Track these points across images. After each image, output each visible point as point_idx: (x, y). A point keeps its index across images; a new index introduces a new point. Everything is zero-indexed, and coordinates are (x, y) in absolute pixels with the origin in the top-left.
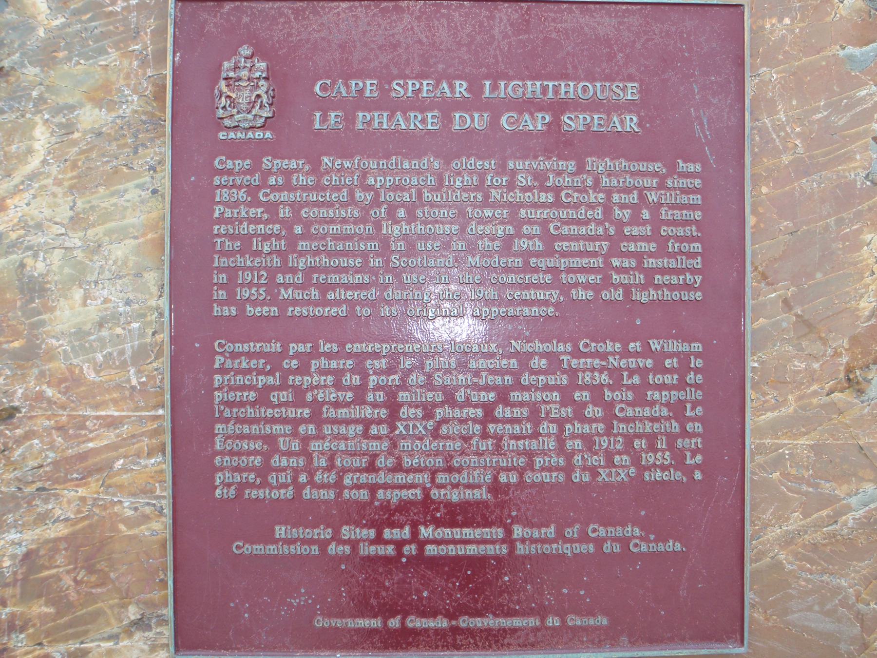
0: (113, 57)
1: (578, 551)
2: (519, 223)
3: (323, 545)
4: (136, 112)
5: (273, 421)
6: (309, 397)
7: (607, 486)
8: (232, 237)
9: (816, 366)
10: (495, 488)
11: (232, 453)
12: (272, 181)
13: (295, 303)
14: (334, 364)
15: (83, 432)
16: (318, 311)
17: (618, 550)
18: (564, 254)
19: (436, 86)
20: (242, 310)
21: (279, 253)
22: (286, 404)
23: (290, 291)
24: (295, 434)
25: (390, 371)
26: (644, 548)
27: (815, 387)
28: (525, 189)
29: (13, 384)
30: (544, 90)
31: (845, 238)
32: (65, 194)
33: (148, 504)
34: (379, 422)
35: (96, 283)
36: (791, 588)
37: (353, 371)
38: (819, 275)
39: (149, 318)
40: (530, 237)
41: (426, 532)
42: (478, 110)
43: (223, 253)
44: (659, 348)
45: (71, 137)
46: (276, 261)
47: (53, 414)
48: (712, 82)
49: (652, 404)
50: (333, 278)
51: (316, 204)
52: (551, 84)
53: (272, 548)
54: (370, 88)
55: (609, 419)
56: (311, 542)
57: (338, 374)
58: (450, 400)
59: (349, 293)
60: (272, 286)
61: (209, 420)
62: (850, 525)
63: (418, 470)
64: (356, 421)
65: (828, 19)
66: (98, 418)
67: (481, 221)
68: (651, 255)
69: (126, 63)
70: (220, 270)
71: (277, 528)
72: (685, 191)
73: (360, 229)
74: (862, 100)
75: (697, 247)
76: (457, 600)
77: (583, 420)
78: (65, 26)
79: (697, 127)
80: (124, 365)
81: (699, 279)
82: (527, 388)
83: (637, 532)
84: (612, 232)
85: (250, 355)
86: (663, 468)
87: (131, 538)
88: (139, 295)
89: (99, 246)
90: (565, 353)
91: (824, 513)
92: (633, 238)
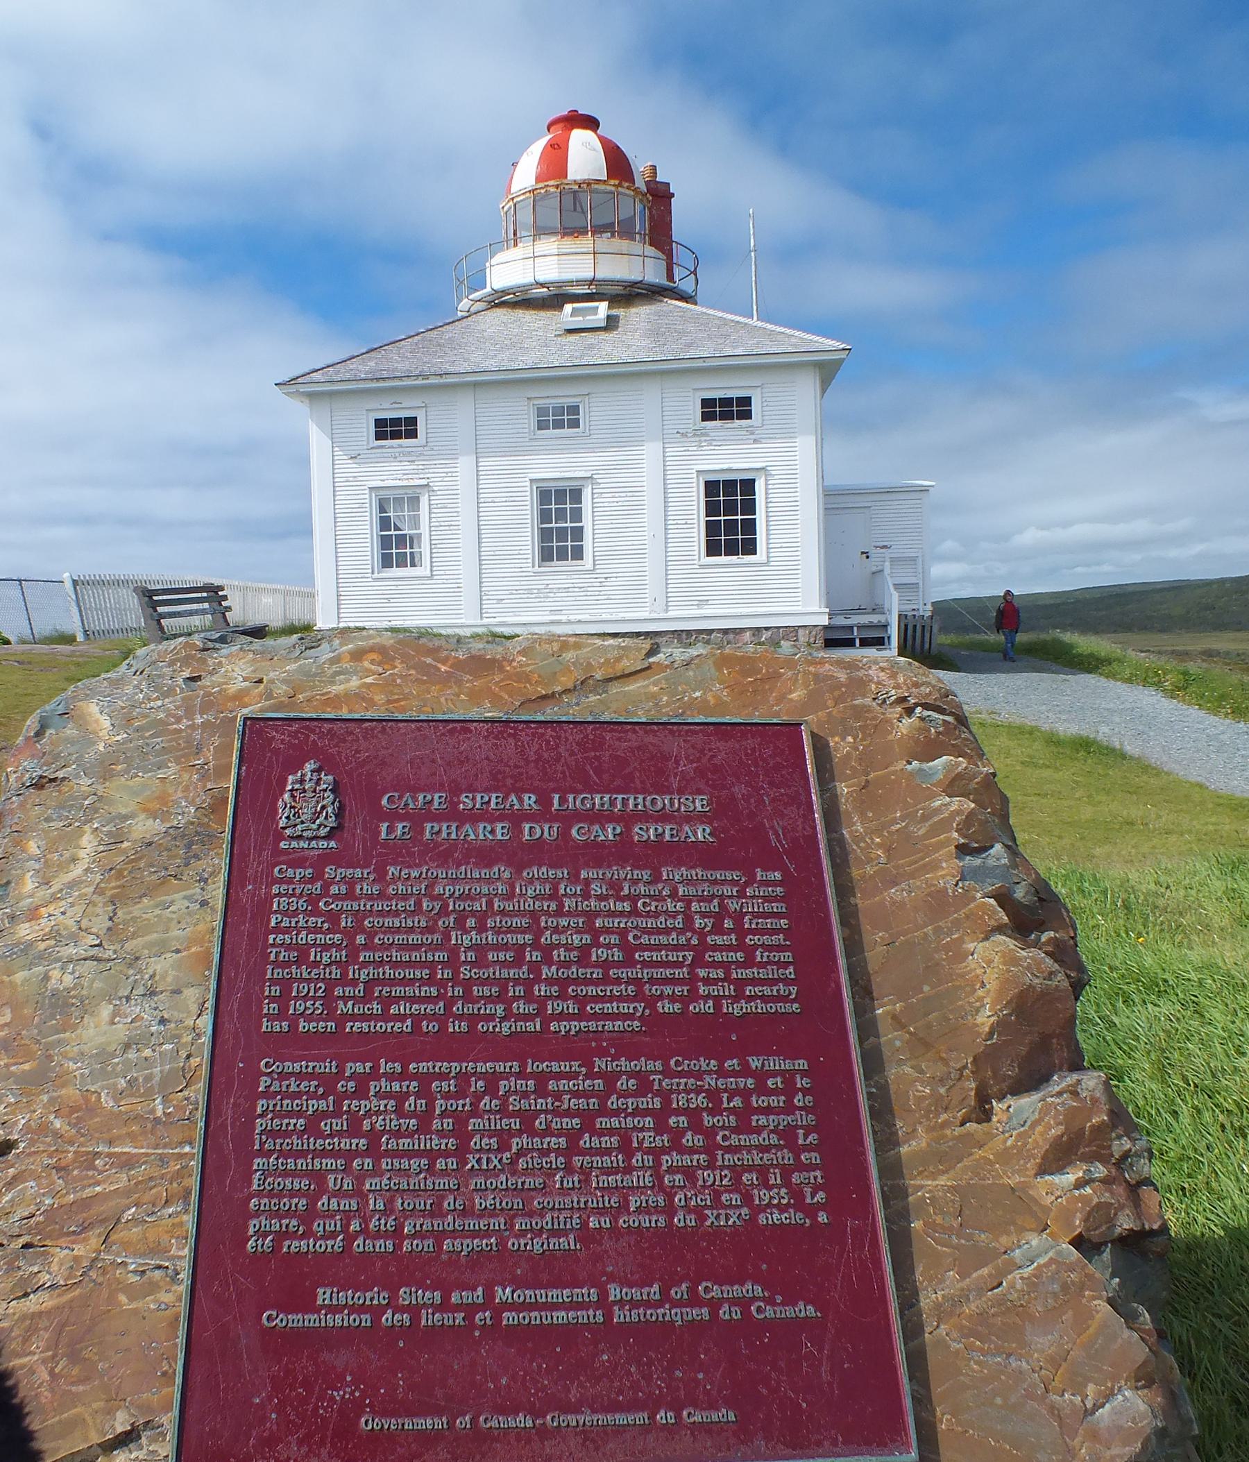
0: (171, 770)
1: (690, 1318)
2: (596, 933)
3: (377, 1312)
4: (192, 823)
5: (324, 1153)
6: (366, 1125)
7: (717, 1232)
8: (288, 948)
9: (942, 1091)
10: (584, 1235)
11: (271, 1194)
12: (334, 890)
13: (354, 1017)
14: (396, 1086)
15: (90, 1173)
16: (380, 1026)
17: (739, 1316)
18: (645, 964)
19: (505, 799)
20: (293, 1025)
21: (338, 963)
22: (340, 1134)
23: (350, 1004)
24: (347, 1169)
25: (460, 1094)
26: (769, 1312)
27: (944, 1117)
28: (601, 898)
29: (13, 1113)
30: (612, 802)
31: (947, 948)
32: (105, 904)
33: (159, 1267)
34: (446, 1154)
35: (128, 998)
36: (963, 1374)
37: (418, 1095)
38: (926, 988)
39: (184, 1040)
40: (608, 946)
41: (503, 1294)
42: (546, 821)
43: (277, 964)
44: (759, 1065)
45: (119, 846)
46: (336, 973)
47: (57, 1150)
48: (782, 795)
49: (758, 1130)
50: (398, 991)
51: (381, 913)
52: (620, 797)
53: (312, 1319)
54: (437, 800)
55: (710, 1149)
56: (362, 1309)
57: (401, 1097)
58: (528, 1128)
59: (415, 1006)
60: (329, 1000)
61: (246, 1153)
62: (1018, 1287)
63: (493, 1213)
64: (419, 1154)
65: (890, 737)
66: (110, 1155)
67: (556, 930)
68: (739, 965)
69: (186, 776)
70: (274, 982)
71: (320, 1291)
72: (767, 899)
73: (428, 938)
74: (938, 811)
75: (787, 956)
76: (544, 1388)
77: (682, 1150)
78: (125, 741)
79: (773, 837)
80: (148, 1095)
81: (794, 989)
82: (616, 1113)
83: (758, 1290)
84: (695, 941)
85: (300, 1076)
86: (782, 1209)
87: (135, 1312)
88: (176, 1014)
89: (137, 959)
90: (656, 1072)
91: (985, 1271)
92: (716, 948)
